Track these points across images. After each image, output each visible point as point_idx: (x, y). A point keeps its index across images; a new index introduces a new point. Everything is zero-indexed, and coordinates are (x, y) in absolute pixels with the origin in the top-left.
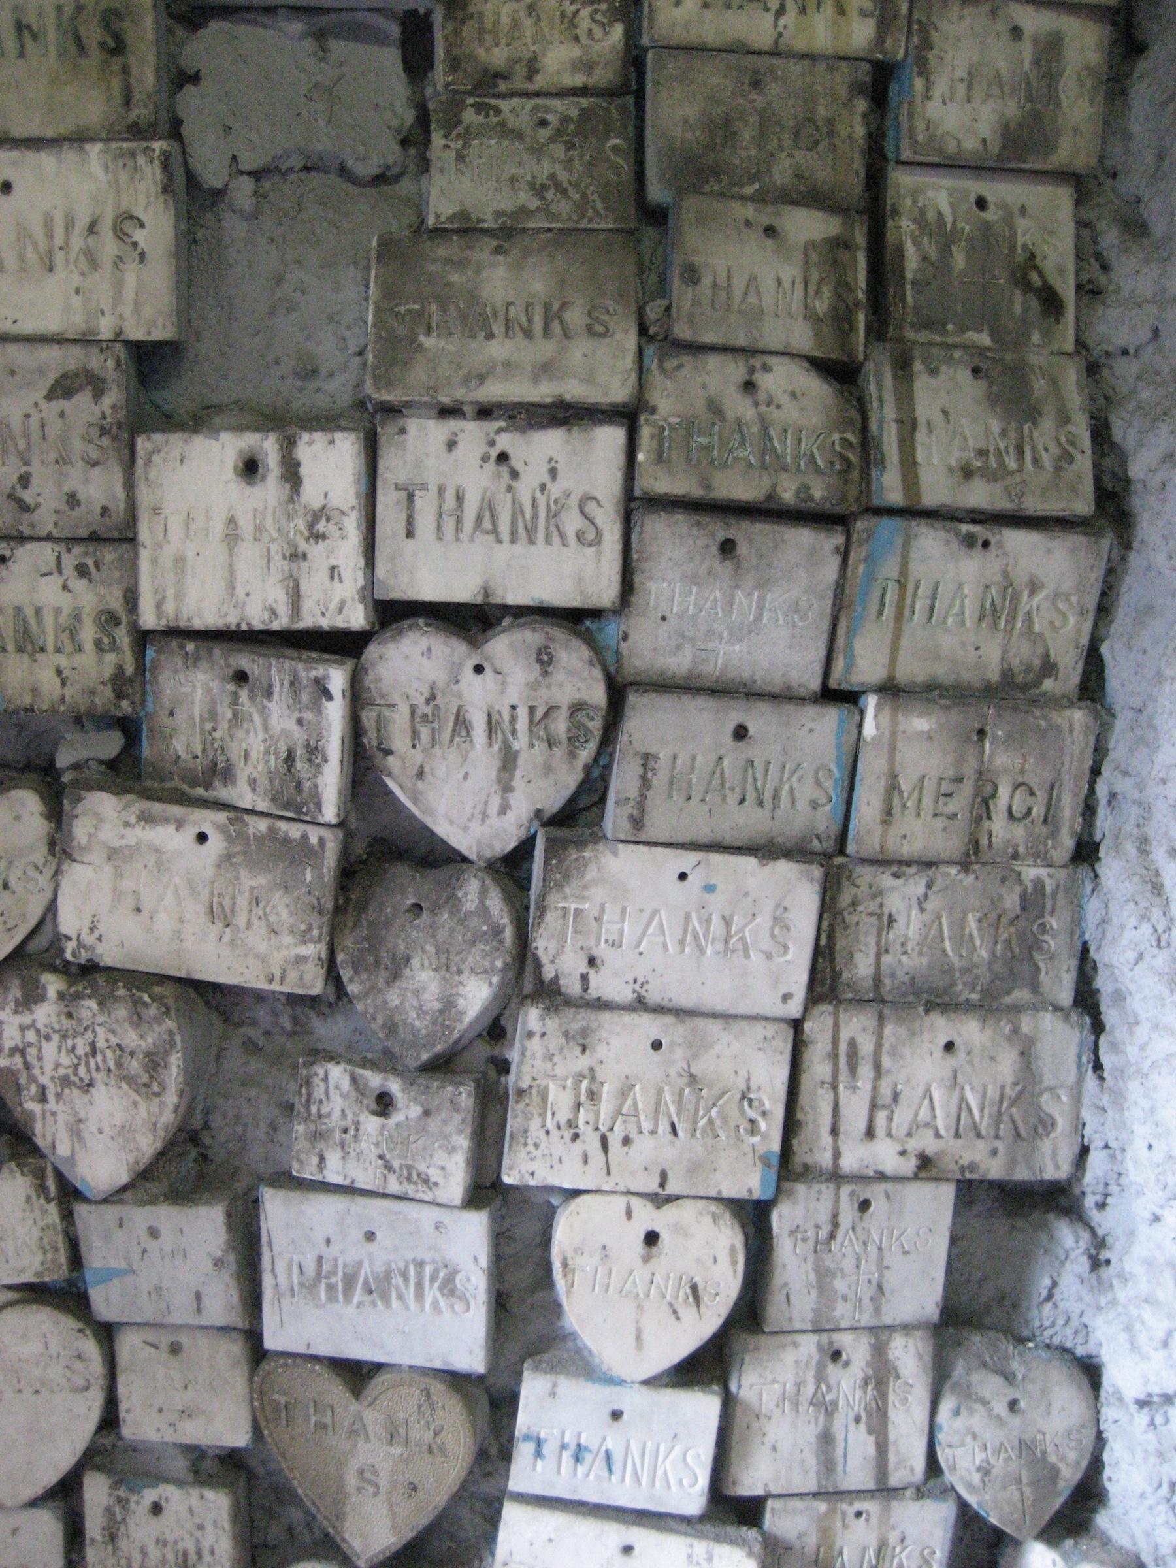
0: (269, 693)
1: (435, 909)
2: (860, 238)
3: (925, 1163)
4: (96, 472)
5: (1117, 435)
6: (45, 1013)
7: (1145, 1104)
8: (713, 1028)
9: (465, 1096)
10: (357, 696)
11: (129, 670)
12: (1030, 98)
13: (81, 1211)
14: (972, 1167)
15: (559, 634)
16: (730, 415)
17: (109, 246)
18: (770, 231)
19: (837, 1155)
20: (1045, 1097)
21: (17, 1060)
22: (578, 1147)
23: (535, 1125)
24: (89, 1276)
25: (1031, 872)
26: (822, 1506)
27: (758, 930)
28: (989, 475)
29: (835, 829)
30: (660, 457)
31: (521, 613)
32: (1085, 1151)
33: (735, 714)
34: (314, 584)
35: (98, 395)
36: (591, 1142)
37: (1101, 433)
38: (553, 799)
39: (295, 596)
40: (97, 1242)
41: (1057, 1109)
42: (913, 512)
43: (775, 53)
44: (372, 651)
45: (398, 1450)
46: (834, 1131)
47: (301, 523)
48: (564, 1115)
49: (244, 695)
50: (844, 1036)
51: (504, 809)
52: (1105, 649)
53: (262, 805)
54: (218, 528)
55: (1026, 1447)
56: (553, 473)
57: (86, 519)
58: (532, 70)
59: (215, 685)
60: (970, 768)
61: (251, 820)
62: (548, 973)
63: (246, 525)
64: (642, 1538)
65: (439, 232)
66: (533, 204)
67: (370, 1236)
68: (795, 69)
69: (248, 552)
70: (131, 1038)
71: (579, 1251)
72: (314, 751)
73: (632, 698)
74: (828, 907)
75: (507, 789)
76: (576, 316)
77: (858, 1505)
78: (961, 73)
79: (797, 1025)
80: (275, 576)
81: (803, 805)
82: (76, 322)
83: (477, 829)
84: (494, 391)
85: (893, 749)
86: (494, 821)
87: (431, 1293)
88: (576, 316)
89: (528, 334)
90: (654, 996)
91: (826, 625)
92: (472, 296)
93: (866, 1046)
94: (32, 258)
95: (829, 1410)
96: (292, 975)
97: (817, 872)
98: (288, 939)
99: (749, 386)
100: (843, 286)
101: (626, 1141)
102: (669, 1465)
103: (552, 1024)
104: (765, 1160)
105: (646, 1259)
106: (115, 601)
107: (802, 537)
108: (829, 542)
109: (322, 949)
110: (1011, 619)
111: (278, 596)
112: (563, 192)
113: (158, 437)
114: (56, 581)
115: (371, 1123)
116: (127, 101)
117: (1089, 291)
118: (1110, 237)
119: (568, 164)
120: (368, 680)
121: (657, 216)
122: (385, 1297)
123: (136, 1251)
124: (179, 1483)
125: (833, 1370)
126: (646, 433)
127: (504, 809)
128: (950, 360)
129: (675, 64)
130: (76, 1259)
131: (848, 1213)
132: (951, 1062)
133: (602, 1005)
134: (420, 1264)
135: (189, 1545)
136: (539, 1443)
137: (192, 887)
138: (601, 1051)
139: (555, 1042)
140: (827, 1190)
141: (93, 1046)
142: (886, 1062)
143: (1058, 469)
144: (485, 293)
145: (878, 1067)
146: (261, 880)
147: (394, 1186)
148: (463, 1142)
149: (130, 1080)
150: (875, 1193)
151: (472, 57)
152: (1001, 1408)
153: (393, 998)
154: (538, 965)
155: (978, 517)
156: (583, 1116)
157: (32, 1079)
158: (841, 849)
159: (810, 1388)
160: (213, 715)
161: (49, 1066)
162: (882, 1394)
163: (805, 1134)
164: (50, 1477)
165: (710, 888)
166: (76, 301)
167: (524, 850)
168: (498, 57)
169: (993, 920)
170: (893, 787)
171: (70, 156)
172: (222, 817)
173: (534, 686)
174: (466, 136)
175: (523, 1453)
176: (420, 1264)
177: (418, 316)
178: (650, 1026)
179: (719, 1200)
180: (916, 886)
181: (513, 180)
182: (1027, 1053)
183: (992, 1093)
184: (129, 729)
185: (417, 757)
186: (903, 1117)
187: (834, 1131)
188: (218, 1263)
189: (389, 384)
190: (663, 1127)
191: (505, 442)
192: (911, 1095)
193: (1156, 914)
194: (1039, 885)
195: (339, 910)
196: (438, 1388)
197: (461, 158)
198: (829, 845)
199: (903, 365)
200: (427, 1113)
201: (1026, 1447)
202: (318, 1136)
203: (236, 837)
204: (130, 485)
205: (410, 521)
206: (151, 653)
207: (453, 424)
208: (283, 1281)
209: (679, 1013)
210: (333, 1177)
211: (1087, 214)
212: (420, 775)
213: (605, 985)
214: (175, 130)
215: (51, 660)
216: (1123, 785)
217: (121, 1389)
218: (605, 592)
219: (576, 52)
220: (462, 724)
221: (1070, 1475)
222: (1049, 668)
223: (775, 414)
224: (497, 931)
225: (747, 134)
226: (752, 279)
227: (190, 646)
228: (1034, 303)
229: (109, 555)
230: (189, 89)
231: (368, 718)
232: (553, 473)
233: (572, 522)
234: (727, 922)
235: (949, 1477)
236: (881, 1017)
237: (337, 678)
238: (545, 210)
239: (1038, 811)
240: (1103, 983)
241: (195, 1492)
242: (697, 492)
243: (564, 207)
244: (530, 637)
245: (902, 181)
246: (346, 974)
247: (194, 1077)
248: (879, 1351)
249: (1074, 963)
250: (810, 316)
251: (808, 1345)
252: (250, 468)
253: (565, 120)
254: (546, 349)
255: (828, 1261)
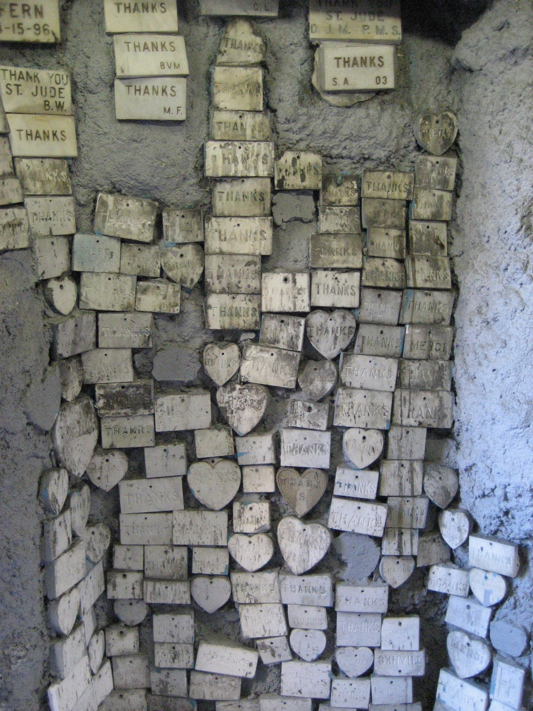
0: (288, 324)
1: (319, 369)
2: (404, 235)
3: (420, 423)
4: (254, 281)
5: (456, 272)
6: (235, 394)
7: (463, 405)
8: (377, 393)
9: (327, 407)
10: (306, 325)
11: (258, 320)
12: (437, 207)
13: (237, 439)
14: (430, 425)
15: (347, 312)
16: (380, 270)
17: (259, 237)
18: (387, 234)
19: (402, 421)
20: (445, 410)
21: (227, 405)
22: (349, 418)
23: (341, 413)
24: (238, 454)
25: (441, 362)
26: (400, 499)
27: (385, 373)
28: (430, 281)
29: (400, 353)
30: (367, 278)
31: (339, 308)
32: (454, 422)
33: (380, 329)
34: (299, 303)
35: (255, 266)
36: (352, 417)
37: (452, 272)
38: (344, 346)
39: (295, 305)
40: (241, 445)
41: (448, 412)
42: (416, 288)
43: (387, 199)
44: (309, 316)
45: (309, 488)
46: (401, 416)
47: (296, 291)
48: (346, 411)
49: (283, 325)
50: (403, 396)
51: (334, 348)
52: (455, 315)
53: (286, 348)
54: (279, 292)
55: (443, 488)
56: (346, 281)
57: (251, 290)
58: (340, 202)
59: (277, 323)
60: (427, 340)
61: (283, 351)
62: (343, 382)
63: (285, 292)
64: (362, 505)
65: (322, 234)
66: (341, 229)
67: (305, 439)
68: (392, 202)
69: (285, 297)
70: (255, 397)
71: (349, 440)
72: (297, 336)
73: (361, 326)
74: (399, 369)
75: (335, 344)
76: (350, 251)
77: (408, 499)
78: (423, 203)
79: (393, 393)
80: (291, 301)
81: (394, 347)
82: (252, 251)
83: (329, 352)
84: (335, 266)
85: (412, 336)
86: (332, 351)
87: (318, 451)
88: (350, 251)
89: (341, 255)
90: (364, 387)
91: (398, 311)
92: (330, 247)
93: (407, 398)
94: (243, 239)
95: (401, 477)
96: (289, 384)
97: (397, 361)
98: (289, 376)
99: (383, 264)
100: (401, 244)
101: (359, 417)
102: (368, 488)
103: (344, 392)
104: (387, 421)
105: (363, 442)
106: (256, 306)
107: (394, 293)
108: (398, 295)
109: (295, 378)
110: (435, 310)
111: (291, 305)
112: (346, 226)
113: (267, 274)
114: (245, 302)
115: (307, 414)
116: (264, 209)
117: (450, 243)
118: (454, 233)
119: (347, 221)
120: (309, 322)
121: (364, 230)
122: (308, 452)
123: (250, 448)
124: (257, 503)
125: (402, 469)
126: (364, 274)
127: (334, 348)
128: (422, 259)
129: (368, 201)
130: (236, 451)
131: (404, 434)
132: (425, 401)
133: (354, 388)
134: (316, 444)
135: (259, 516)
136: (340, 484)
137: (269, 364)
138: (354, 398)
139: (345, 396)
140: (400, 429)
141: (246, 400)
142: (412, 401)
143: (444, 280)
144: (332, 246)
145: (410, 402)
146: (284, 364)
147: (311, 427)
148: (326, 417)
149: (254, 407)
150: (410, 429)
151: (328, 199)
152: (438, 479)
153: (311, 388)
154: (341, 380)
155: (428, 289)
156: (350, 411)
157: (230, 408)
158: (402, 357)
159: (397, 473)
160: (276, 329)
161: (234, 405)
162: (412, 475)
163: (395, 417)
164: (226, 502)
165: (376, 364)
166: (252, 247)
167: (338, 356)
168: (333, 199)
169: (433, 372)
170: (412, 344)
171: (252, 219)
172: (277, 350)
173: (342, 323)
174: (327, 215)
175: (337, 486)
176: (316, 444)
177: (320, 251)
178: (363, 393)
179: (378, 430)
180: (417, 364)
181: (337, 224)
182: (441, 400)
183: (434, 409)
184: (257, 332)
185: (318, 337)
186: (415, 413)
187: (401, 416)
188: (269, 449)
189: (315, 264)
190: (367, 414)
191: (337, 275)
192: (417, 409)
193: (464, 367)
194: (442, 365)
195: (299, 370)
196: (319, 472)
197: (326, 219)
198: (399, 356)
199: (413, 260)
200: (319, 411)
201: (443, 488)
202: (296, 417)
203: (279, 354)
204: (261, 283)
205: (318, 291)
206: (263, 316)
207: (327, 272)
208: (286, 450)
209: (369, 390)
210: (298, 426)
211: (449, 228)
212: (318, 341)
213: (356, 384)
214: (271, 214)
215: (242, 318)
216: (460, 343)
217: (244, 481)
218: (356, 304)
219: (348, 198)
220: (327, 331)
221: (453, 495)
222: (443, 319)
223: (388, 270)
224: (333, 373)
225: (382, 214)
226: (384, 244)
227: (272, 315)
228: (439, 247)
229: (255, 297)
230: (274, 206)
231: (308, 329)
232: (346, 281)
233: (350, 291)
234: (379, 371)
235: (427, 494)
236: (410, 393)
237: (303, 321)
238: (343, 230)
239: (442, 349)
240: (456, 386)
241: (260, 504)
242: (374, 285)
243: (347, 230)
244: (341, 313)
245: (412, 223)
246: (300, 383)
247: (268, 407)
248: (411, 465)
249: (450, 382)
250: (395, 250)
251: (396, 463)
252: (286, 280)
253: (346, 211)
254: (344, 257)
255: (400, 444)
